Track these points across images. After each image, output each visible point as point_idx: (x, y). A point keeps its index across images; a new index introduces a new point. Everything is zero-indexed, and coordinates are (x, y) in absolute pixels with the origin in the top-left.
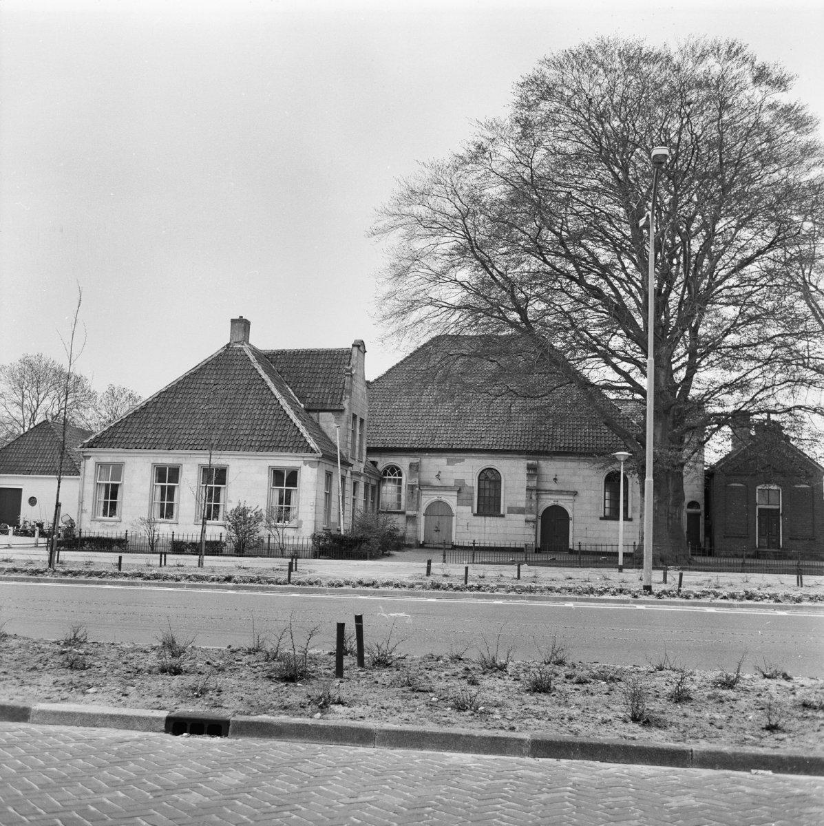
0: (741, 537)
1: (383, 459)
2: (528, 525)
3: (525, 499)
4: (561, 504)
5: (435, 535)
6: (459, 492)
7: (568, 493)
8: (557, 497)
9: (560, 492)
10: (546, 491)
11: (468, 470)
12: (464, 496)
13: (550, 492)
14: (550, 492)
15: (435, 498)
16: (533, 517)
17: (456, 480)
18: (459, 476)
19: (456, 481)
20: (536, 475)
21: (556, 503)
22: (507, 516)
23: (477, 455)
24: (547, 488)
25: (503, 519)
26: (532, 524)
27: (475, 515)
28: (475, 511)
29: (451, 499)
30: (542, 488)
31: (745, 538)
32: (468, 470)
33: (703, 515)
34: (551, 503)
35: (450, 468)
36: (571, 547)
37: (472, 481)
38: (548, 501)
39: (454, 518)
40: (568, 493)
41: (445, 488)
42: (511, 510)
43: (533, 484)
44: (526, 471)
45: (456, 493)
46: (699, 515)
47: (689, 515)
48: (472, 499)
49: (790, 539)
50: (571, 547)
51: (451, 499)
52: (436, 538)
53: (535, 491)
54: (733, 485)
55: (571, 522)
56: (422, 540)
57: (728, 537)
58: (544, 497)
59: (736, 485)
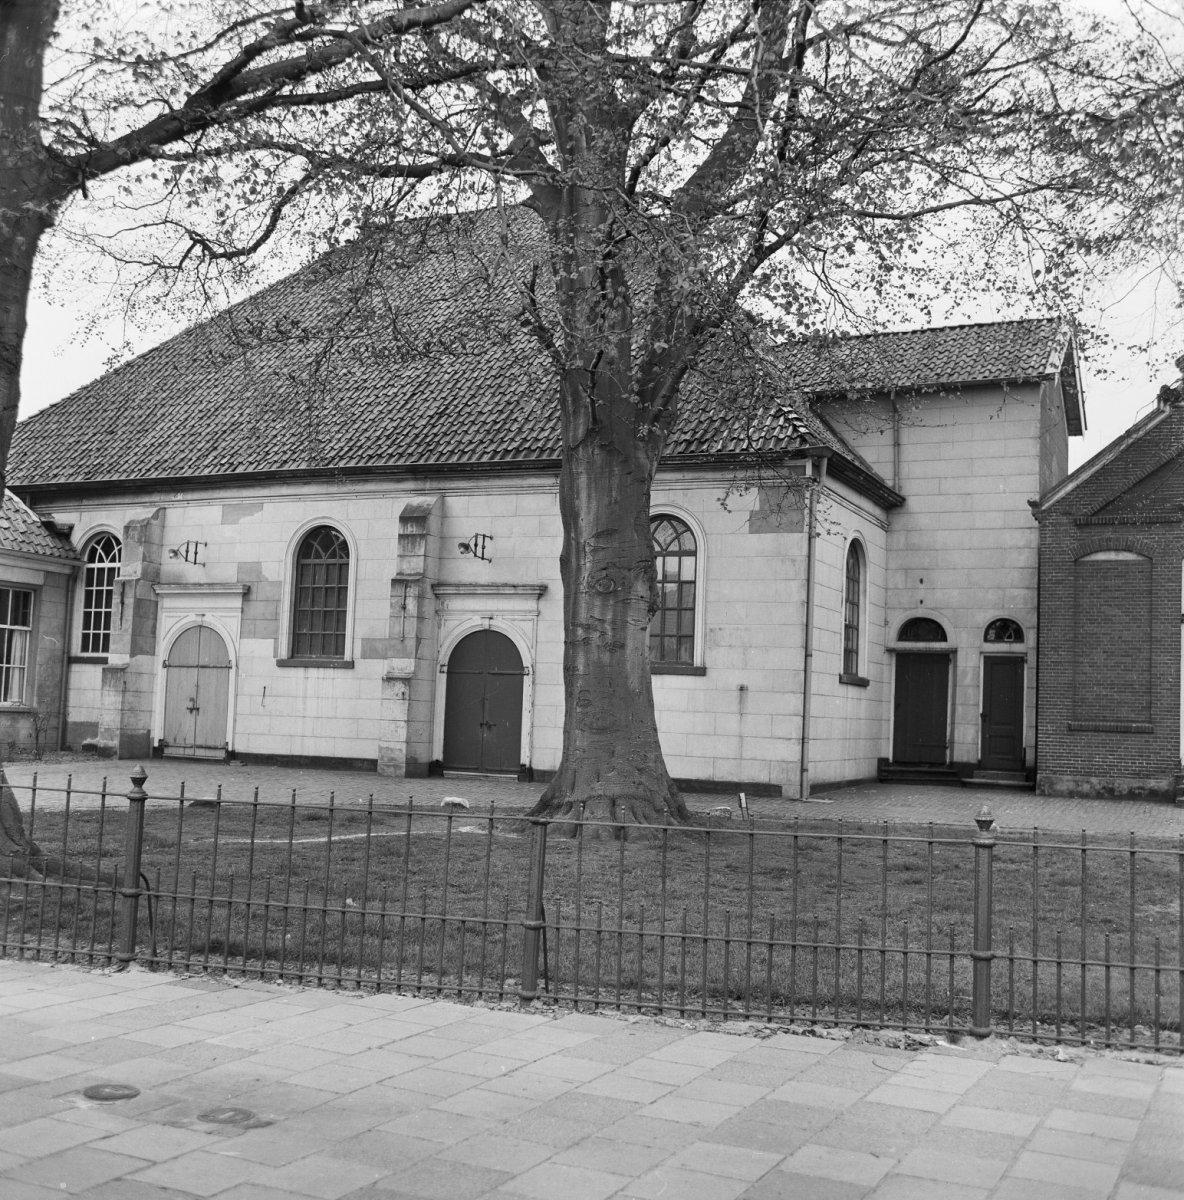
0: (1127, 731)
1: (86, 516)
2: (389, 693)
3: (387, 611)
4: (500, 625)
5: (189, 720)
6: (246, 594)
7: (515, 589)
8: (491, 604)
9: (495, 590)
10: (458, 585)
11: (257, 535)
12: (257, 608)
13: (472, 590)
14: (472, 590)
15: (192, 619)
16: (404, 665)
17: (241, 567)
18: (248, 554)
19: (241, 567)
20: (422, 536)
21: (486, 624)
22: (360, 664)
23: (696, 475)
24: (466, 579)
25: (349, 673)
26: (400, 687)
27: (281, 664)
28: (284, 653)
29: (224, 618)
30: (453, 579)
31: (1140, 732)
32: (257, 535)
33: (1032, 659)
34: (476, 623)
35: (228, 531)
36: (525, 759)
37: (279, 569)
38: (464, 618)
39: (232, 672)
40: (515, 589)
41: (212, 590)
42: (371, 650)
43: (415, 565)
44: (396, 528)
45: (238, 603)
46: (1018, 661)
47: (991, 663)
48: (276, 618)
49: (1070, 729)
50: (525, 759)
51: (224, 618)
52: (190, 732)
53: (424, 590)
54: (1101, 556)
55: (527, 681)
56: (157, 735)
57: (1081, 729)
58: (455, 604)
59: (1112, 556)
